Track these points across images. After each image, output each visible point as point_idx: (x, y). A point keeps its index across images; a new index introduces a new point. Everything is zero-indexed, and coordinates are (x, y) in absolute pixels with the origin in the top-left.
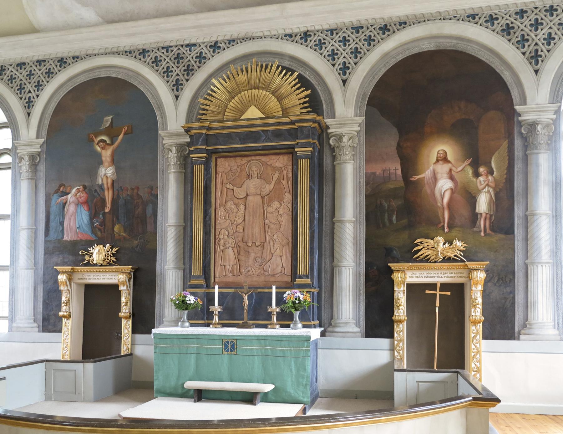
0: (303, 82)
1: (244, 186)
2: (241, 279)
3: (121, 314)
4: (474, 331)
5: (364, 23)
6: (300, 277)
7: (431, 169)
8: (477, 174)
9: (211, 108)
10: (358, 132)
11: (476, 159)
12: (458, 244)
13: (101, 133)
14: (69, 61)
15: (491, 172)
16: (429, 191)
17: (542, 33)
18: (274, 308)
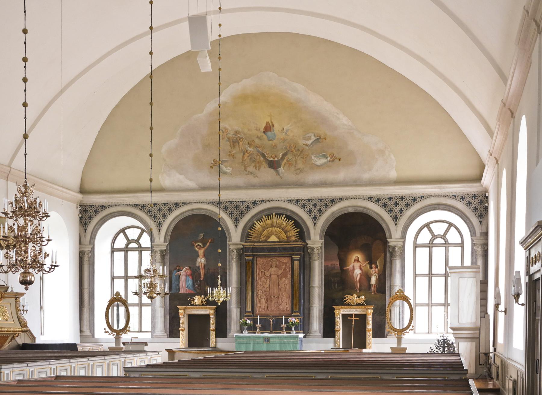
0: (297, 225)
1: (270, 271)
2: (268, 312)
3: (180, 329)
4: (369, 334)
5: (323, 198)
6: (295, 312)
7: (352, 265)
8: (371, 268)
9: (254, 235)
10: (321, 247)
11: (371, 261)
12: (362, 297)
13: (198, 241)
14: (180, 204)
15: (377, 267)
16: (351, 274)
17: (398, 208)
18: (284, 325)
